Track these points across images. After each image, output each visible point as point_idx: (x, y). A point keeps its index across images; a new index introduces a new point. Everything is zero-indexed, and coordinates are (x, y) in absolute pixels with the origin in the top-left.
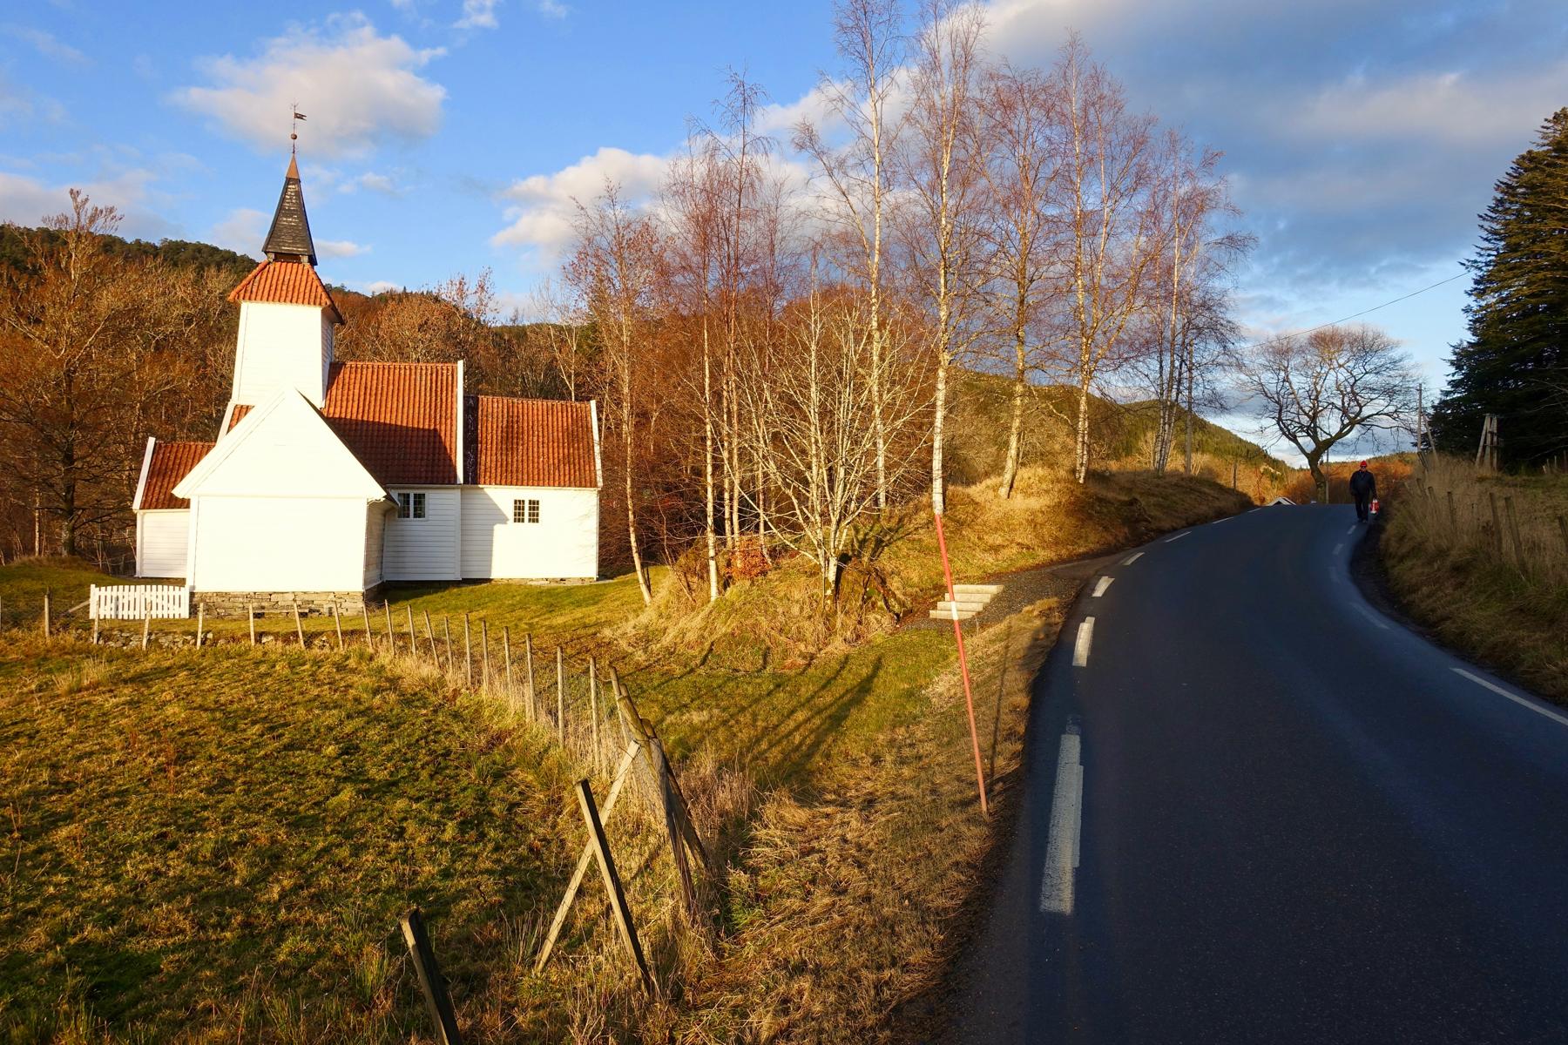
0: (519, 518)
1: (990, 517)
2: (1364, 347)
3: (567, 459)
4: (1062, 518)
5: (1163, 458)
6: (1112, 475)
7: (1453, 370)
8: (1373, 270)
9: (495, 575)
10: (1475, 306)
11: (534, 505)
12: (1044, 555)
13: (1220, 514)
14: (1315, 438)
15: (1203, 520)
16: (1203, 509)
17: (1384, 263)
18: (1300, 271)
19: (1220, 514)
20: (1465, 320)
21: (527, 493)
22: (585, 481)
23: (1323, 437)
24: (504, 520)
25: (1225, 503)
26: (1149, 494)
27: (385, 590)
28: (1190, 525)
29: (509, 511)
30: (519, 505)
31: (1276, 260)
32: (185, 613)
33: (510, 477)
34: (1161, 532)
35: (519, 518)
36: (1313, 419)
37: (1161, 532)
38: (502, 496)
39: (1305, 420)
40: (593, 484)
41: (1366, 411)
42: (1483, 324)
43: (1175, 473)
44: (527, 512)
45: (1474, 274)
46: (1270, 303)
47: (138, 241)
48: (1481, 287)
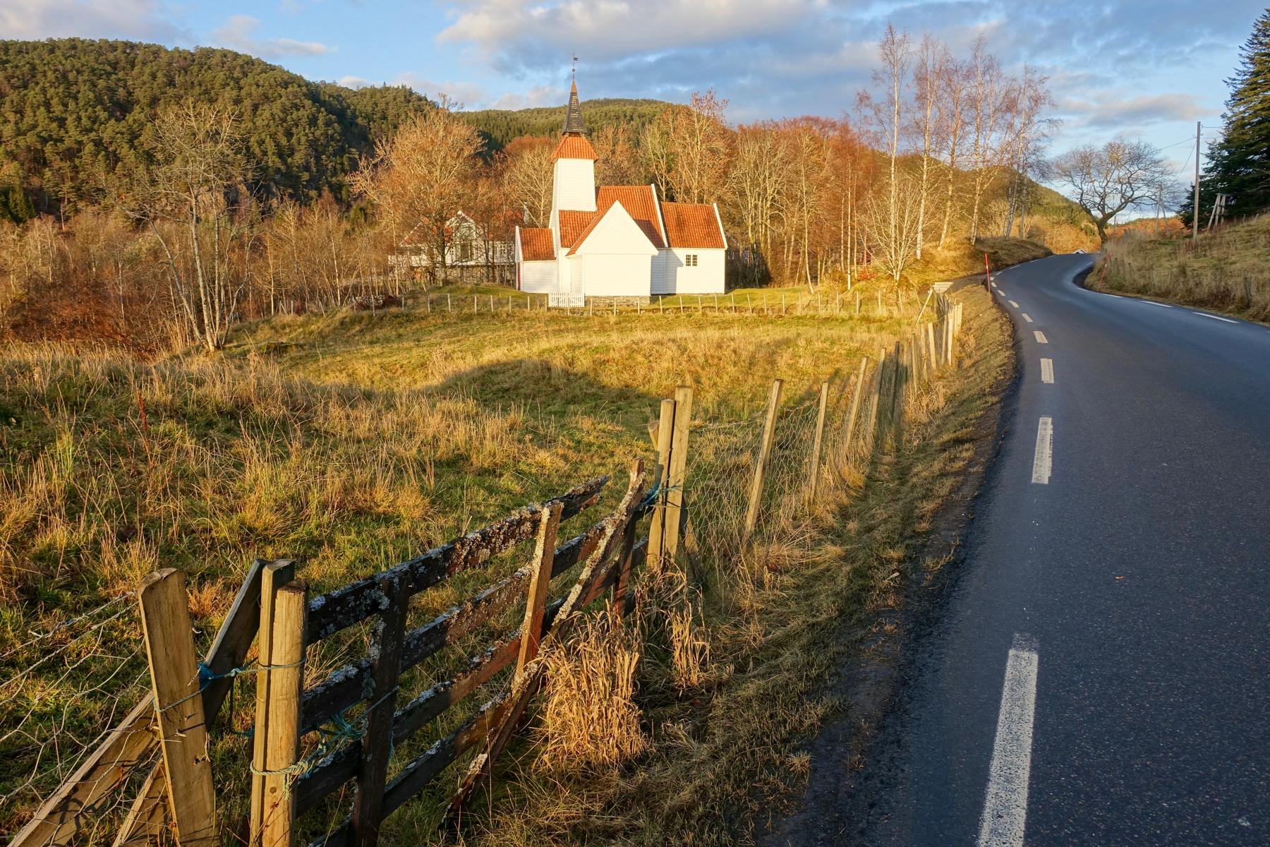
0: (688, 264)
1: (938, 259)
2: (1136, 158)
3: (709, 234)
4: (966, 260)
5: (1009, 231)
6: (987, 239)
7: (1208, 160)
8: (1187, 49)
9: (678, 292)
10: (1230, 114)
11: (695, 257)
12: (962, 274)
13: (1034, 258)
14: (1103, 211)
15: (1026, 260)
16: (1027, 256)
17: (1198, 43)
18: (1123, 52)
19: (1034, 258)
20: (1222, 124)
21: (692, 252)
22: (717, 244)
23: (1108, 211)
24: (681, 265)
25: (1039, 252)
26: (1002, 249)
27: (654, 298)
28: (1020, 262)
29: (684, 261)
30: (688, 258)
31: (1100, 43)
32: (582, 304)
33: (684, 243)
34: (1008, 266)
35: (688, 264)
36: (1103, 199)
37: (1008, 266)
38: (681, 253)
39: (1098, 200)
40: (723, 247)
41: (1137, 194)
42: (1237, 127)
43: (1014, 238)
44: (692, 261)
45: (1231, 90)
46: (1093, 81)
47: (197, 47)
48: (1238, 98)
